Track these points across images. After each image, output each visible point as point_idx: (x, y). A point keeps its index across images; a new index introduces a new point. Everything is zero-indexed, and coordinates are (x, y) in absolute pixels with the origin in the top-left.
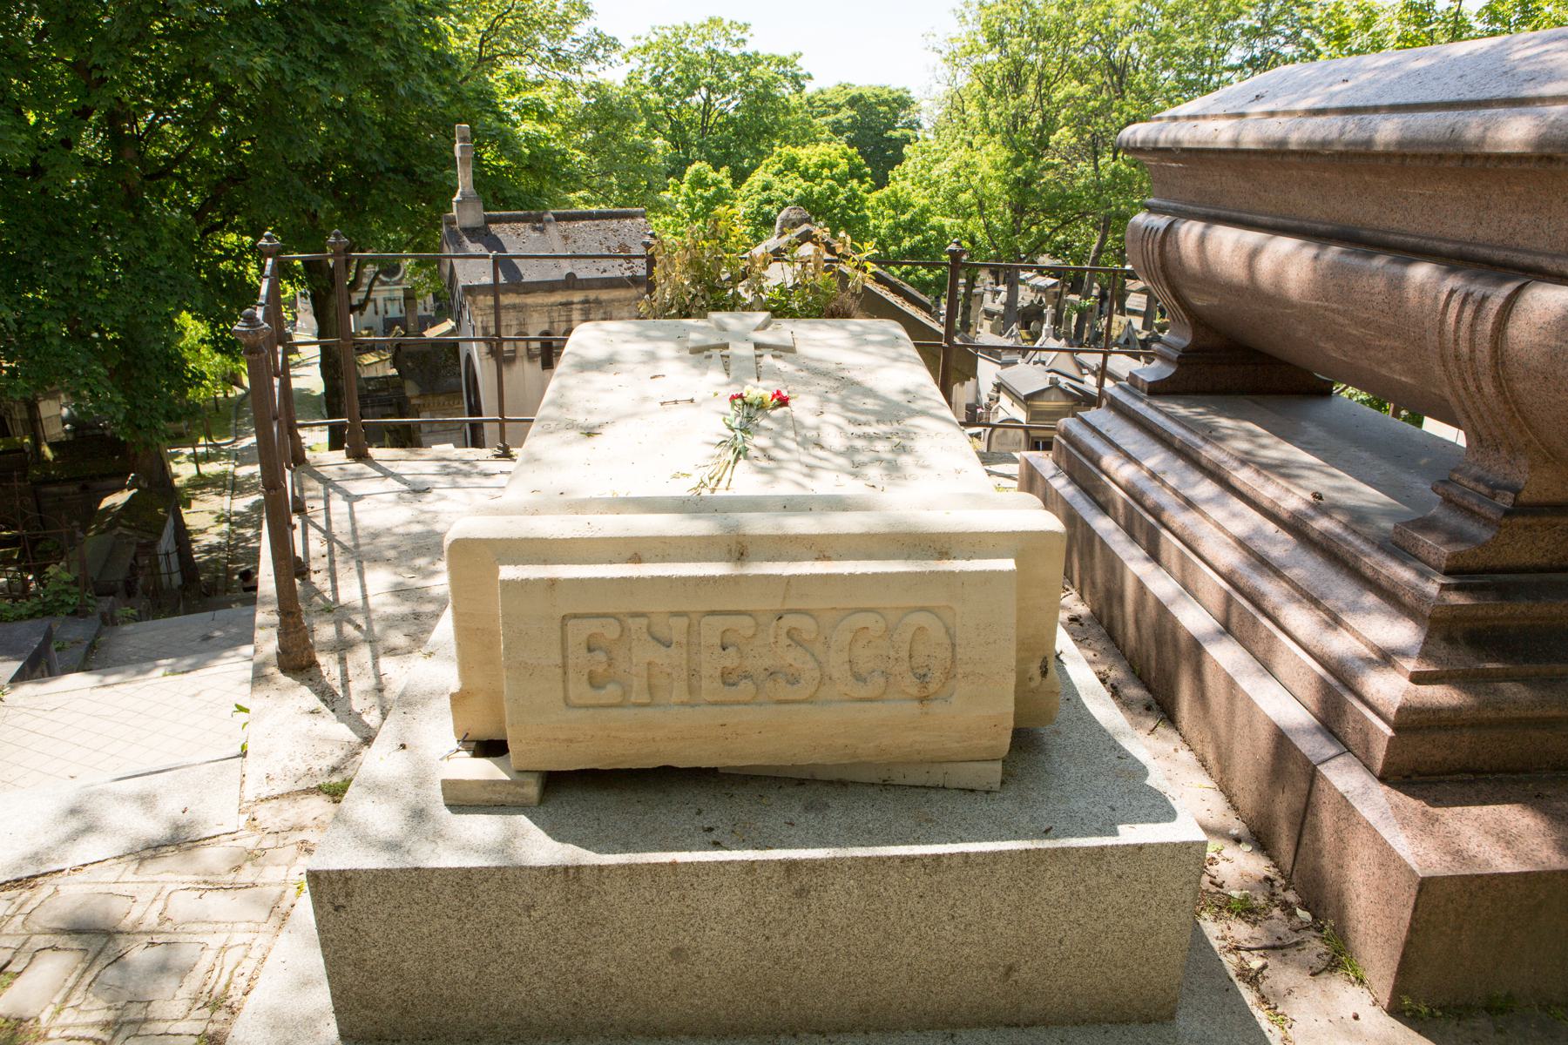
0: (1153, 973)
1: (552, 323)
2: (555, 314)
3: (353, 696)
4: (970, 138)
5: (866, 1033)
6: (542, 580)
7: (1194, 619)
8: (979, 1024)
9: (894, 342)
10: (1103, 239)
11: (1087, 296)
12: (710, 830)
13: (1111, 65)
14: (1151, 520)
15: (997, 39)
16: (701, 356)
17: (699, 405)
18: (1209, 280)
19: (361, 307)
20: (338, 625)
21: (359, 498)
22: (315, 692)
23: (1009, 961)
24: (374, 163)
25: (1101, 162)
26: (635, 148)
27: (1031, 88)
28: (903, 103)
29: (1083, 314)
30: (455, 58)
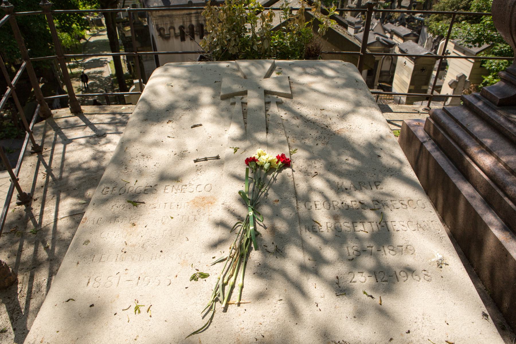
1: (184, 22)
2: (185, 19)
21: (71, 141)
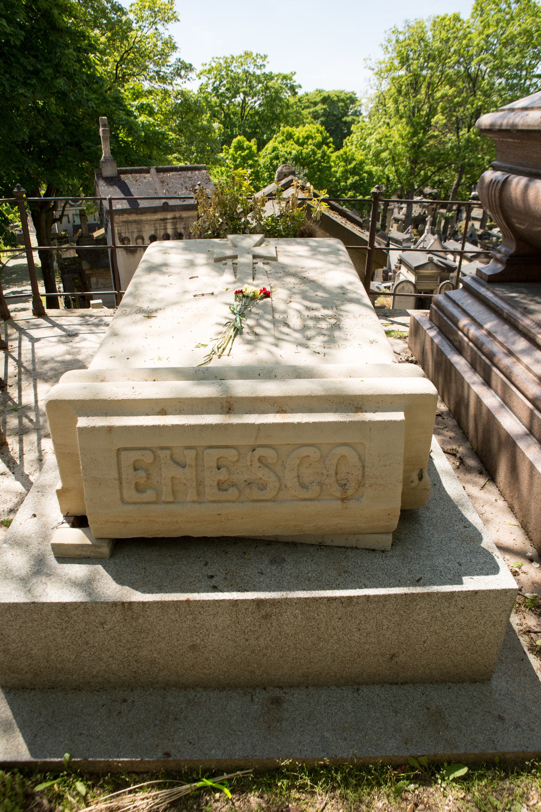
0: (479, 658)
1: (156, 230)
2: (158, 225)
3: (25, 464)
4: (387, 120)
5: (307, 687)
6: (103, 427)
7: (510, 423)
8: (374, 683)
9: (336, 252)
10: (460, 178)
11: (450, 211)
12: (212, 577)
13: (469, 75)
14: (487, 361)
15: (405, 61)
16: (220, 264)
17: (217, 296)
18: (527, 213)
19: (60, 220)
20: (20, 418)
21: (38, 340)
22: (4, 461)
23: (393, 652)
24: (58, 141)
25: (461, 133)
26: (203, 128)
27: (423, 91)
28: (352, 100)
29: (448, 221)
30: (101, 78)
